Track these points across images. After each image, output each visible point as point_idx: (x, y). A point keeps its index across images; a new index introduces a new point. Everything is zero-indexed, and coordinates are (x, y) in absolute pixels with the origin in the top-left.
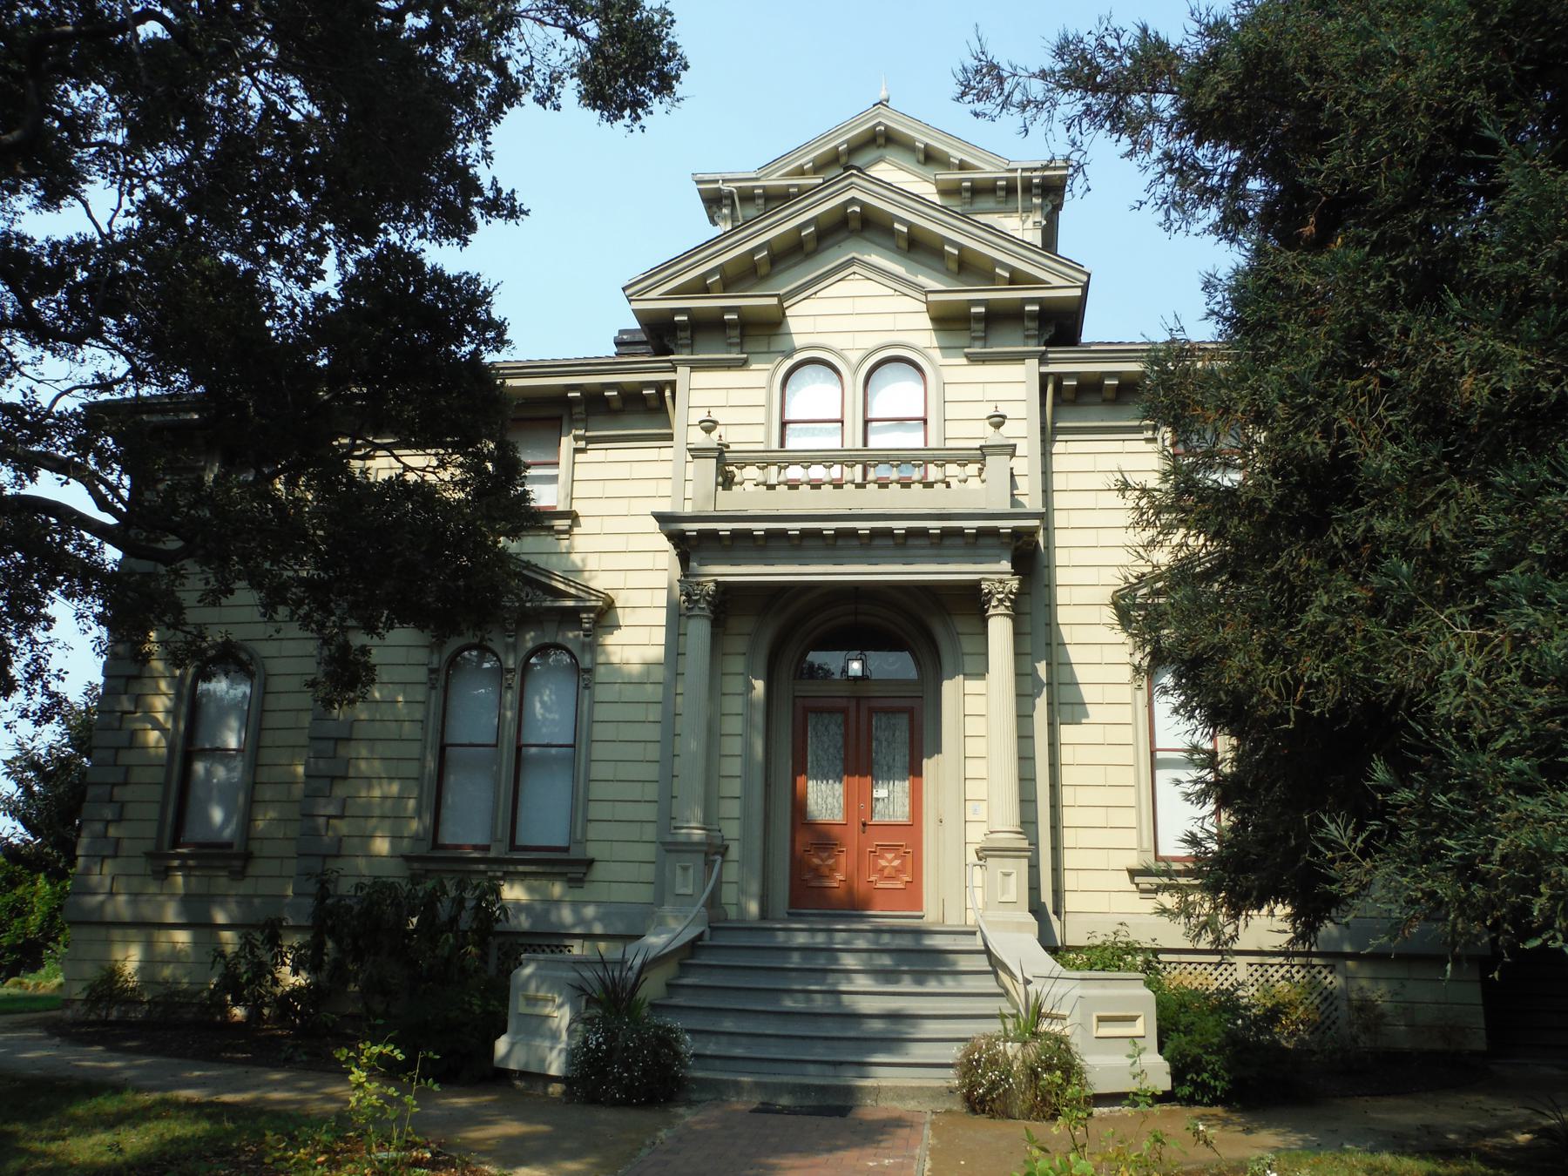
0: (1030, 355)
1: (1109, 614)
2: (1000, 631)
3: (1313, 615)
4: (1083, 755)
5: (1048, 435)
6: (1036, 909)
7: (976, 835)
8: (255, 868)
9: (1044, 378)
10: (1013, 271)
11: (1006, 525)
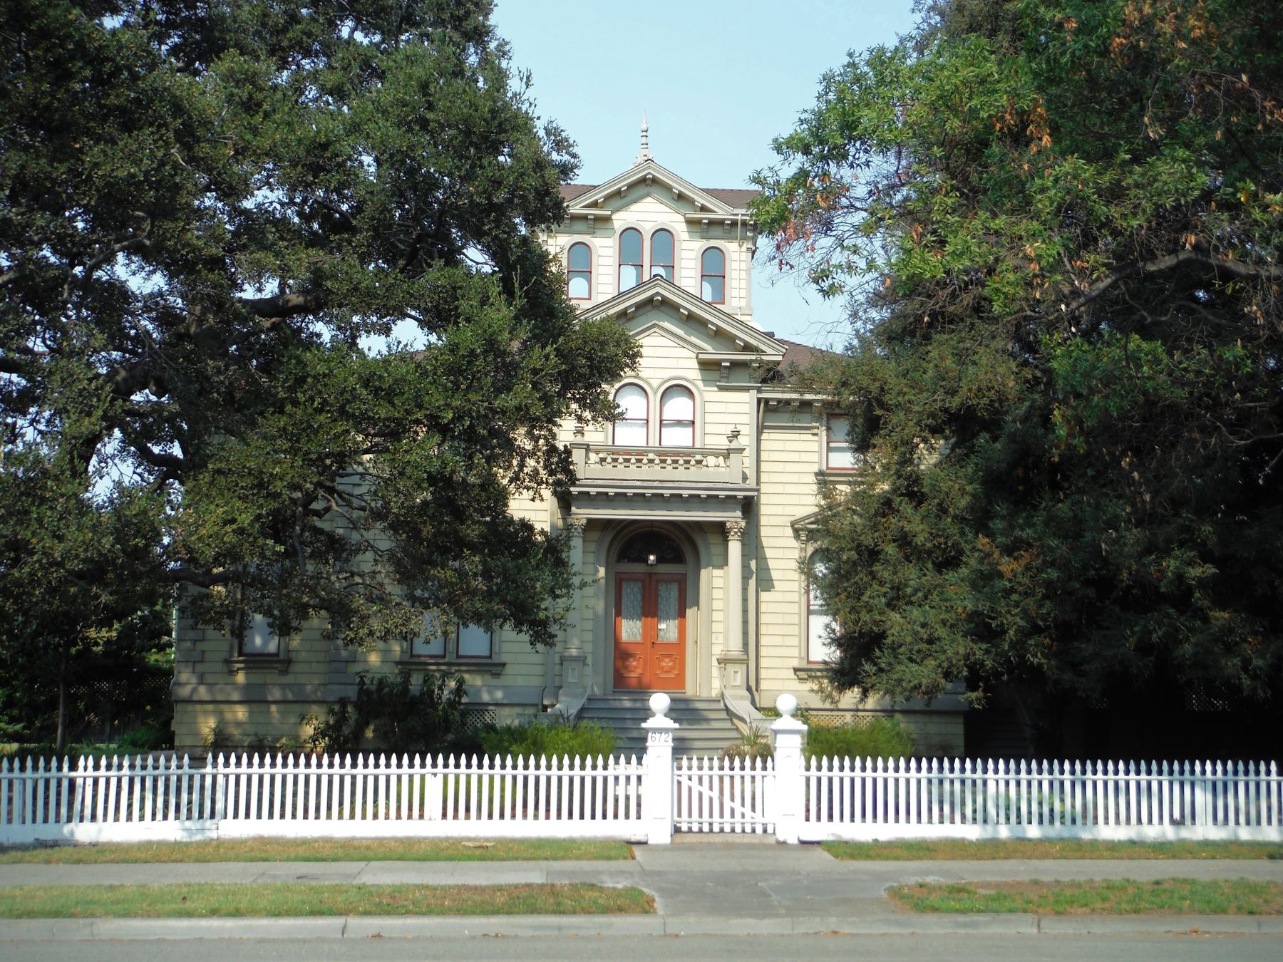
0: (752, 388)
1: (789, 532)
2: (735, 548)
3: (865, 598)
4: (772, 608)
5: (760, 429)
6: (749, 689)
7: (717, 651)
8: (294, 668)
9: (759, 401)
10: (746, 343)
11: (740, 494)
